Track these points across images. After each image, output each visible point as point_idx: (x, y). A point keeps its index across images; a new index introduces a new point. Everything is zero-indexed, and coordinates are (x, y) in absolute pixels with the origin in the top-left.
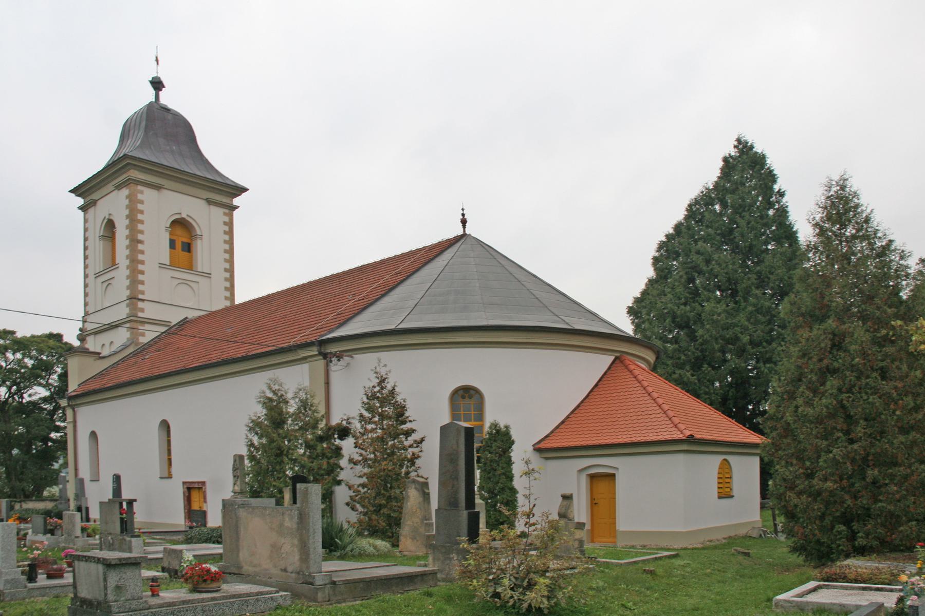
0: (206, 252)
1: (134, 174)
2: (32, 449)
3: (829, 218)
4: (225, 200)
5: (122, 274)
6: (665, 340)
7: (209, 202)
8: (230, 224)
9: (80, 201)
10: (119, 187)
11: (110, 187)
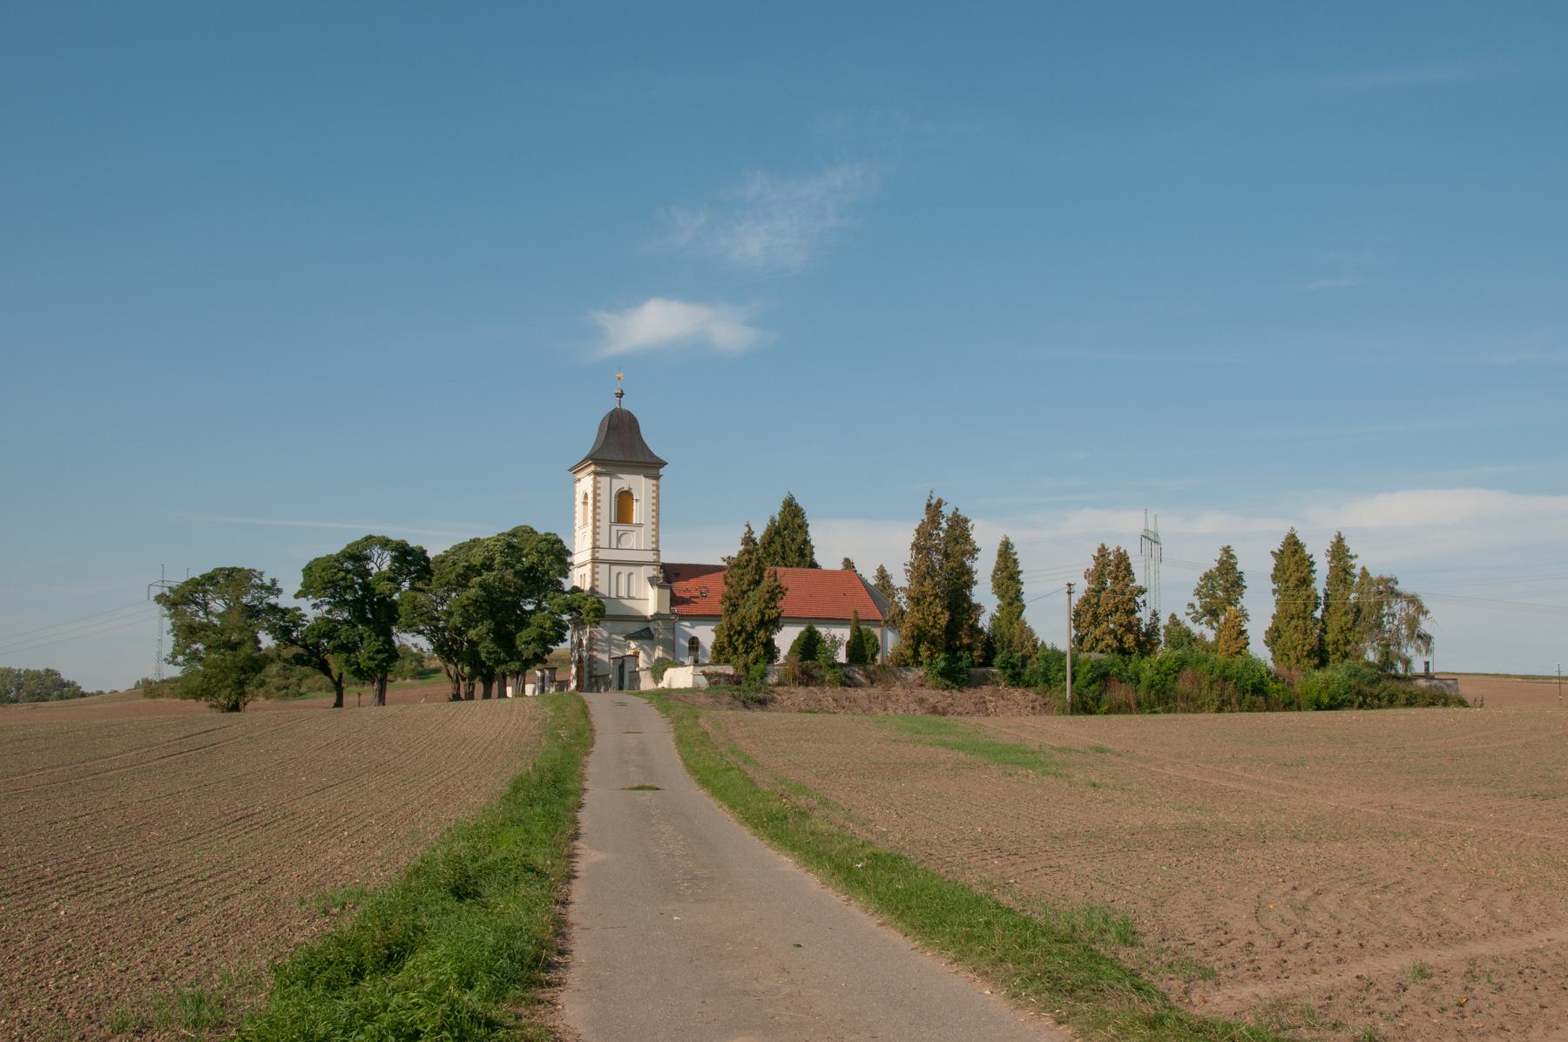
0: (639, 512)
4: (653, 472)
8: (658, 486)
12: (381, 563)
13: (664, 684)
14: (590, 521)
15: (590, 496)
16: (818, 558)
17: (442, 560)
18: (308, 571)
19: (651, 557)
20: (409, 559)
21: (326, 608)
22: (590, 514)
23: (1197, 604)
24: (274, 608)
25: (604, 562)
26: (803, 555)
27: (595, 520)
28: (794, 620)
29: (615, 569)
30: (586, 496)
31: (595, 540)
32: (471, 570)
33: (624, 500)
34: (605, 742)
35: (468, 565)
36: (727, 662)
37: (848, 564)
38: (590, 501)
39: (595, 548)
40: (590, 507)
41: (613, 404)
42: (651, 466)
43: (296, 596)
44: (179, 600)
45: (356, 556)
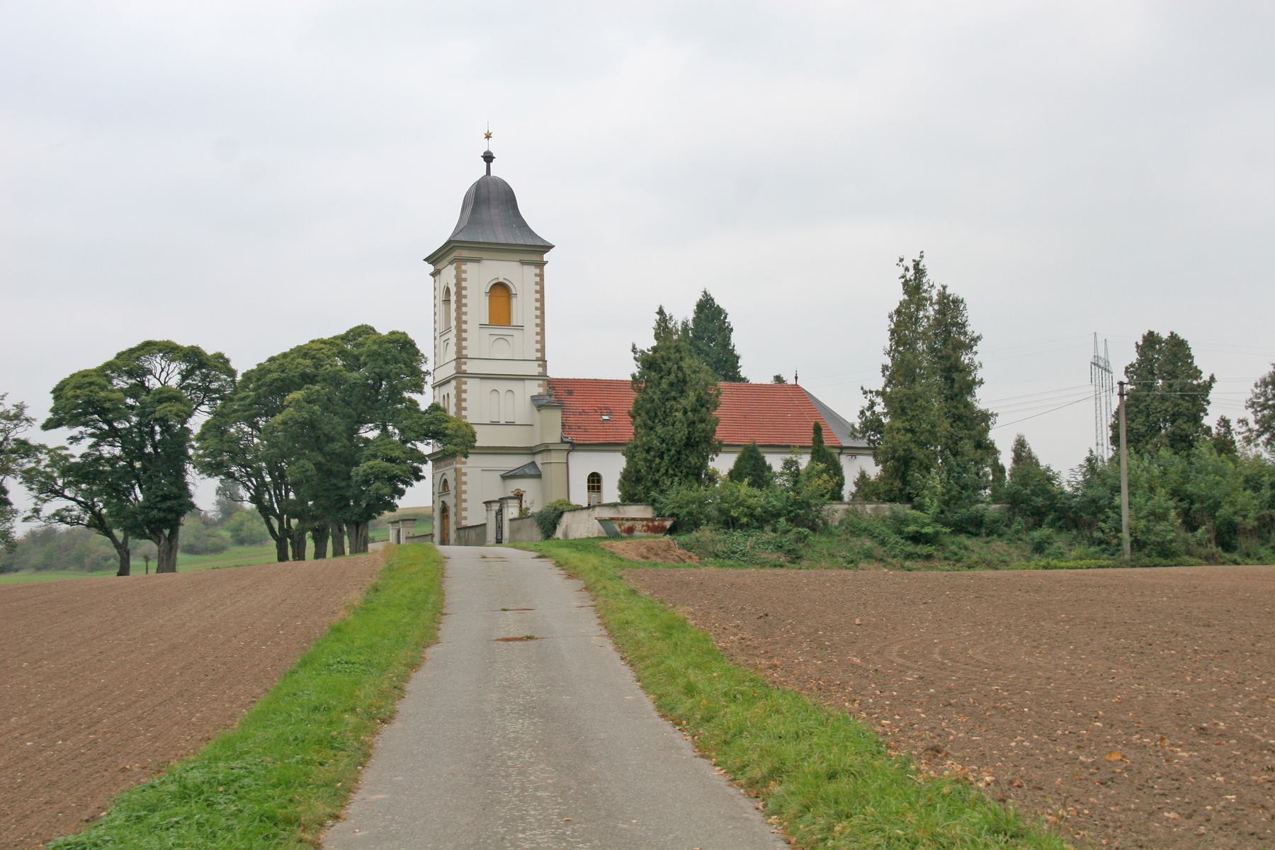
0: (522, 308)
1: (465, 254)
2: (394, 427)
3: (897, 344)
4: (534, 258)
5: (452, 335)
6: (327, 490)
7: (523, 263)
8: (541, 276)
9: (431, 268)
10: (451, 263)
11: (445, 262)
14: (453, 323)
15: (453, 290)
16: (743, 373)
18: (58, 392)
19: (534, 369)
21: (91, 441)
22: (453, 314)
23: (1251, 419)
24: (25, 448)
26: (727, 364)
28: (731, 447)
31: (460, 348)
32: (285, 386)
33: (501, 290)
34: (462, 628)
35: (276, 380)
37: (778, 379)
38: (453, 298)
39: (460, 358)
40: (453, 306)
42: (534, 251)
43: (46, 427)
44: (174, 570)
45: (131, 362)
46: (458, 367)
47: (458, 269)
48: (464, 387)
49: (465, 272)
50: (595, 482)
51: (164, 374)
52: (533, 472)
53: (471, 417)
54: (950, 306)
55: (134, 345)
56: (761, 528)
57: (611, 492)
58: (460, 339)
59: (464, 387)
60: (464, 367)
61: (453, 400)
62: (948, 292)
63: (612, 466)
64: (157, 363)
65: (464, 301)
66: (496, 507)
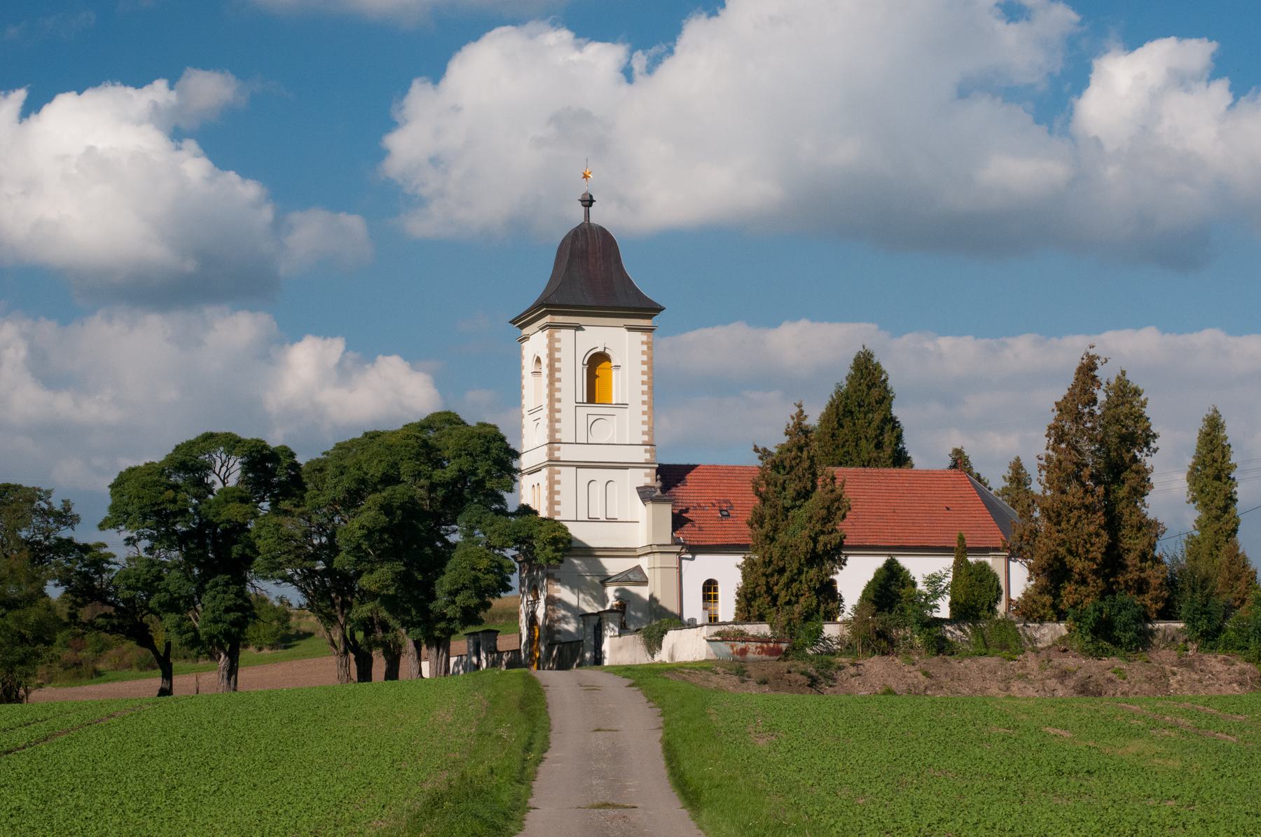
7: (631, 329)
10: (542, 329)
12: (228, 473)
13: (662, 656)
15: (545, 361)
17: (318, 467)
19: (641, 455)
20: (268, 469)
21: (146, 543)
24: (66, 546)
25: (568, 464)
27: (552, 399)
29: (586, 474)
30: (538, 360)
31: (553, 431)
36: (761, 618)
39: (553, 442)
41: (577, 215)
43: (102, 527)
45: (189, 463)
46: (551, 452)
47: (551, 337)
48: (557, 477)
49: (559, 340)
50: (710, 589)
51: (224, 469)
52: (638, 578)
53: (564, 513)
54: (1125, 393)
55: (192, 437)
56: (759, 520)
57: (727, 608)
58: (553, 420)
59: (557, 477)
60: (557, 454)
61: (544, 493)
62: (1127, 377)
63: (728, 571)
64: (219, 457)
65: (557, 375)
66: (595, 620)
